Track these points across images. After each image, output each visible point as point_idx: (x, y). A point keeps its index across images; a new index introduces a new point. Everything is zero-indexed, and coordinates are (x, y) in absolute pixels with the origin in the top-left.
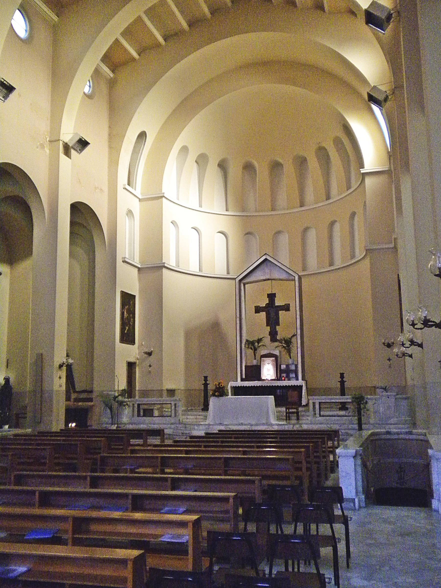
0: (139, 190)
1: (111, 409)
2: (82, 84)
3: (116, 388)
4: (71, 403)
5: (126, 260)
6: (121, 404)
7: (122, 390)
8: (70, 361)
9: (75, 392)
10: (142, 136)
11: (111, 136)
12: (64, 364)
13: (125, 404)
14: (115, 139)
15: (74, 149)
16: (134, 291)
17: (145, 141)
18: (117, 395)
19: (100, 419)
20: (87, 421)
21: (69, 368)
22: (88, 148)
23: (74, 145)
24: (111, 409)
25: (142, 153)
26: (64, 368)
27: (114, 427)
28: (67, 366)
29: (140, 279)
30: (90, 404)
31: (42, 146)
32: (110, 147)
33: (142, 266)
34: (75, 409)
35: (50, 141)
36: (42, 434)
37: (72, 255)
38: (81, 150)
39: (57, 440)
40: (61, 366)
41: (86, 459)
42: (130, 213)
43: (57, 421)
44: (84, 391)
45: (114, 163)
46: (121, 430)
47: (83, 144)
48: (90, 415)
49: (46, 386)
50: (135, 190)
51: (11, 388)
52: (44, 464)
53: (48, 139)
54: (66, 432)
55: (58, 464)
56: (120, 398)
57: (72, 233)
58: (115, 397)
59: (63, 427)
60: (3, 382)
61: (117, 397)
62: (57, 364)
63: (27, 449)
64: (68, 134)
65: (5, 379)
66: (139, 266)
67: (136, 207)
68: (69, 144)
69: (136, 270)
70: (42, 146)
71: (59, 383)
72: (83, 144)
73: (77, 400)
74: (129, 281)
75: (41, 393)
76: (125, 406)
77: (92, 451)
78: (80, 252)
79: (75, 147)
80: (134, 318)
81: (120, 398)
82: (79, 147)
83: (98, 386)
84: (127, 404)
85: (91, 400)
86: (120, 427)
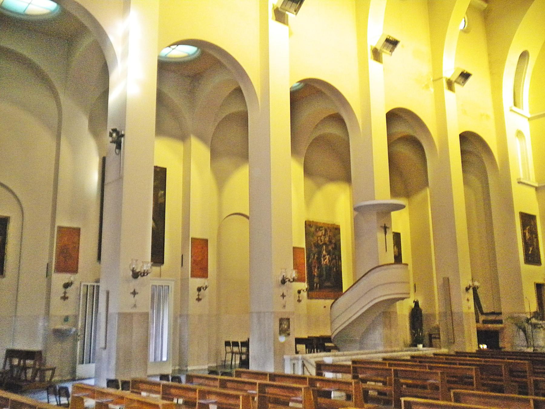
0: (526, 109)
1: (524, 331)
2: (458, 20)
3: (527, 310)
4: (480, 325)
5: (522, 180)
6: (535, 326)
7: (534, 312)
8: (476, 284)
9: (482, 313)
10: (524, 55)
11: (491, 64)
12: (470, 286)
13: (540, 326)
14: (495, 66)
15: (459, 83)
16: (533, 209)
17: (527, 66)
18: (529, 317)
19: (512, 341)
20: (498, 342)
21: (475, 289)
22: (471, 79)
23: (458, 78)
24: (524, 331)
25: (525, 72)
26: (471, 291)
27: (530, 350)
28: (473, 289)
29: (538, 199)
30: (501, 326)
31: (427, 87)
32: (492, 74)
33: (540, 185)
34: (486, 331)
35: (434, 81)
36: (458, 354)
37: (466, 182)
38: (464, 82)
39: (474, 360)
40: (467, 289)
41: (512, 381)
42: (519, 134)
43: (472, 345)
44: (493, 313)
45: (497, 88)
46: (538, 353)
47: (465, 76)
48: (501, 336)
49: (455, 309)
50: (523, 109)
51: (420, 311)
52: (472, 384)
53: (432, 79)
54: (480, 352)
55: (483, 385)
56: (534, 321)
57: (464, 162)
58: (528, 320)
59: (477, 349)
60: (413, 305)
61: (530, 319)
62: (463, 287)
63: (496, 375)
64: (450, 71)
65: (414, 302)
66: (537, 185)
67: (526, 127)
68: (451, 79)
69: (533, 190)
70: (427, 87)
71: (467, 306)
72: (465, 76)
73: (485, 322)
74: (526, 201)
75: (449, 313)
76: (539, 328)
77: (515, 373)
78: (475, 181)
79: (458, 81)
80: (537, 237)
81: (534, 321)
82: (461, 80)
83: (506, 309)
84: (542, 327)
85: (500, 322)
86: (537, 350)
